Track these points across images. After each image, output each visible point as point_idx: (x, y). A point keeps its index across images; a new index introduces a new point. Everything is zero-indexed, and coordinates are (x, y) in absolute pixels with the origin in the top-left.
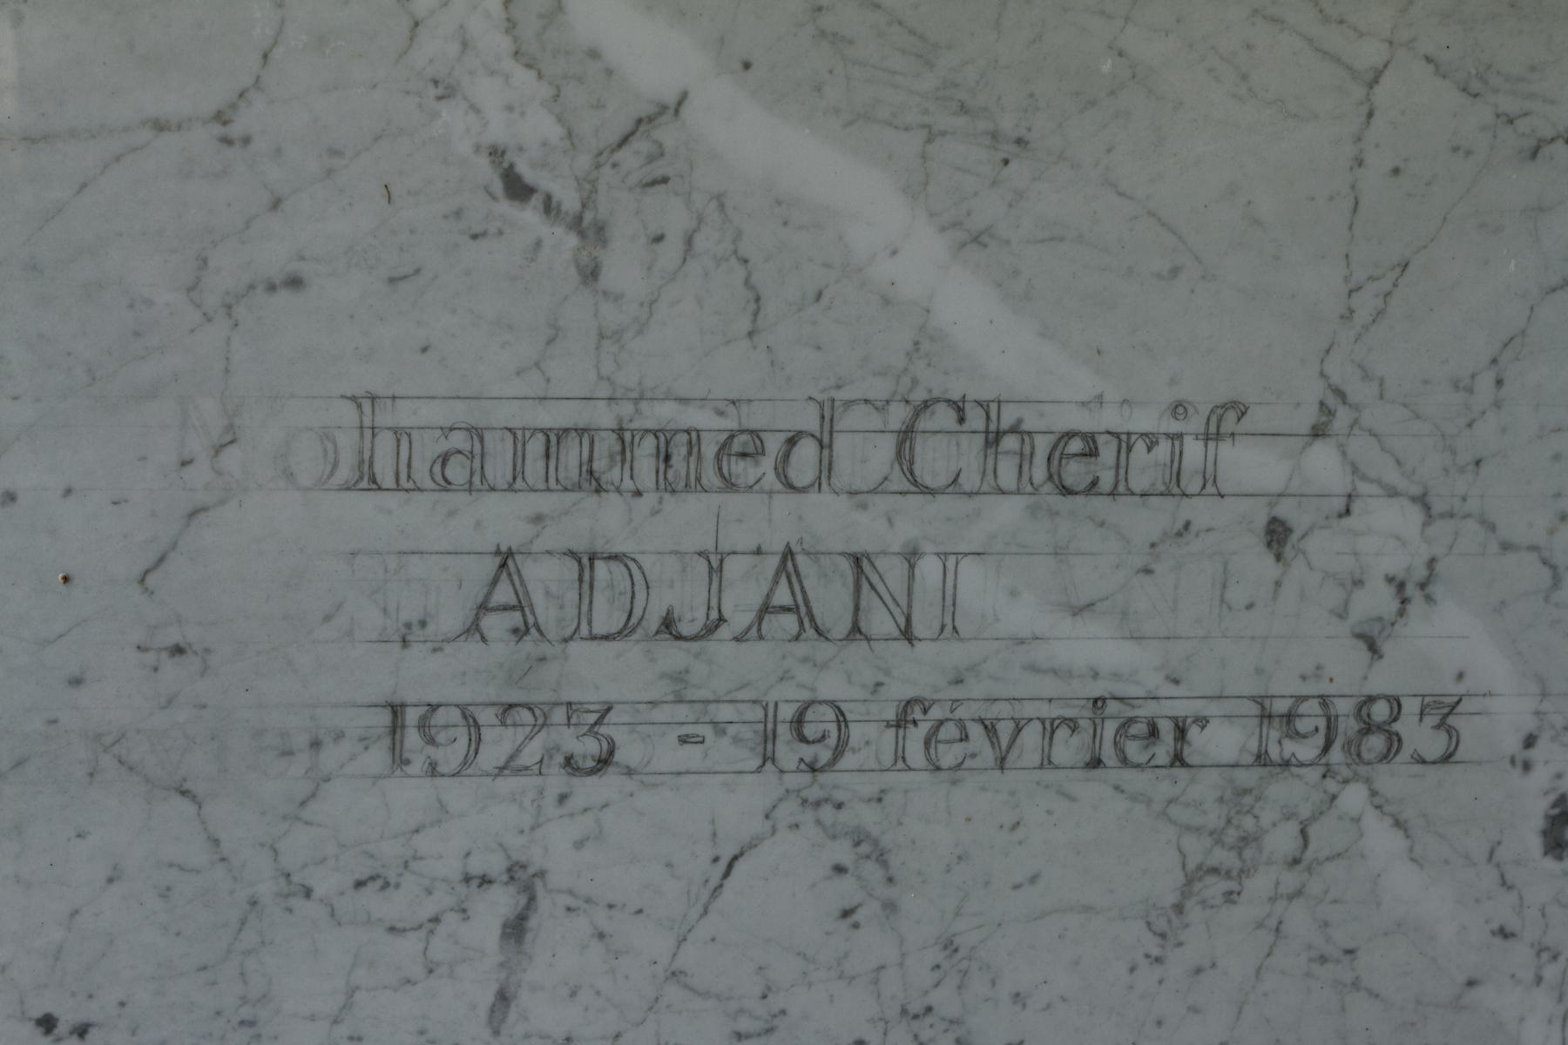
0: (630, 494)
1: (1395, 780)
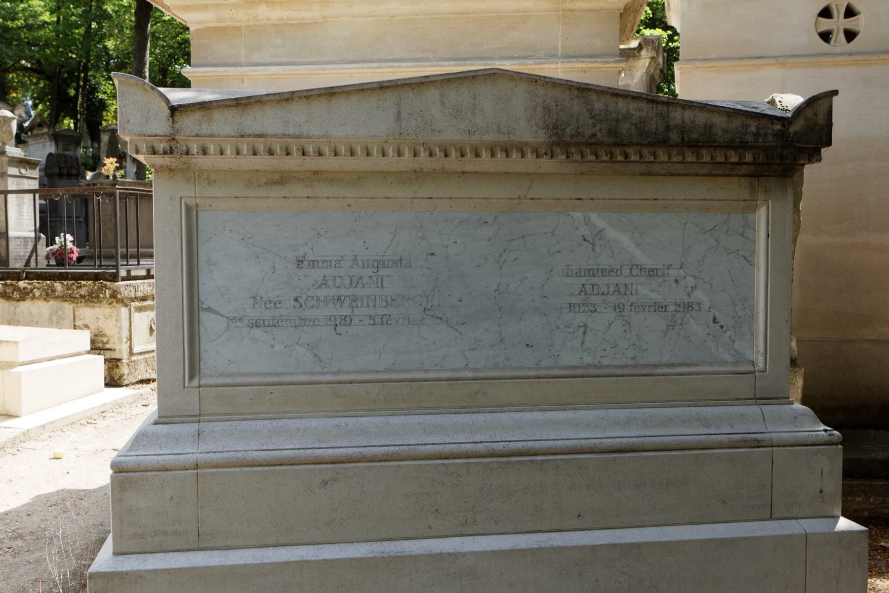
1: (693, 313)
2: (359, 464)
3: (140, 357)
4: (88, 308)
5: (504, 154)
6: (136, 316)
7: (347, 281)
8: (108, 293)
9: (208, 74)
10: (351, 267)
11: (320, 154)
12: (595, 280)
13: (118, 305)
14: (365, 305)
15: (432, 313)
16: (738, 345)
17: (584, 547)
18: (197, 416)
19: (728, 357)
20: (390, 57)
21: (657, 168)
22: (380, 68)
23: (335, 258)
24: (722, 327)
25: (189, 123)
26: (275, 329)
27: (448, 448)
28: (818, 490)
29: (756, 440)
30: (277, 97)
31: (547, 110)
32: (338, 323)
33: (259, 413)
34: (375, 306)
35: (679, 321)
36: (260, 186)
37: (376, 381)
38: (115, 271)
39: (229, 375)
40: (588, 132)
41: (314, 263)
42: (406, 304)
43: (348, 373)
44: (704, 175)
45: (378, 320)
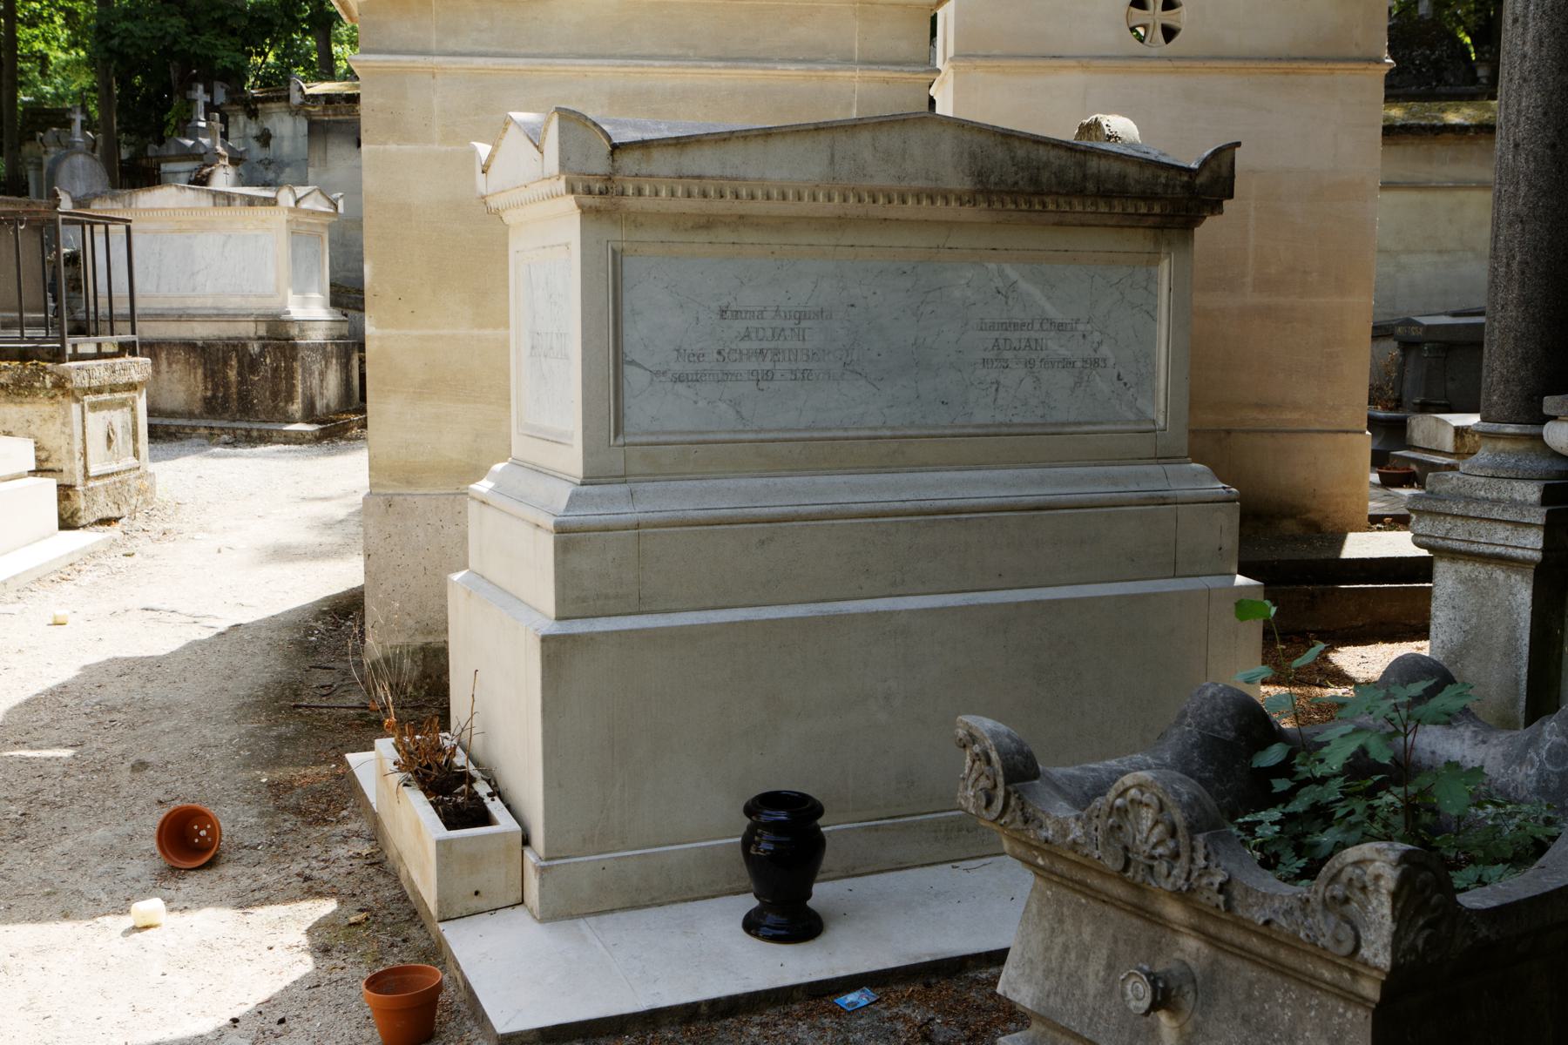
0: (208, 100)
1: (1099, 370)
2: (794, 523)
3: (98, 483)
4: (12, 405)
5: (930, 202)
6: (90, 416)
7: (769, 333)
8: (48, 381)
9: (387, 64)
10: (773, 318)
11: (753, 197)
12: (1008, 334)
13: (66, 400)
14: (787, 359)
15: (851, 368)
16: (1139, 403)
17: (1009, 604)
18: (622, 476)
19: (1131, 416)
20: (637, 52)
21: (1069, 218)
22: (626, 66)
23: (758, 309)
24: (1125, 384)
25: (628, 162)
26: (698, 384)
27: (878, 506)
28: (1217, 547)
29: (1162, 497)
30: (716, 137)
31: (973, 156)
32: (760, 377)
33: (685, 474)
34: (796, 360)
35: (1086, 378)
36: (686, 230)
37: (798, 440)
38: (58, 345)
39: (652, 433)
40: (1010, 181)
41: (737, 314)
42: (826, 358)
43: (770, 431)
44: (1112, 226)
45: (799, 375)
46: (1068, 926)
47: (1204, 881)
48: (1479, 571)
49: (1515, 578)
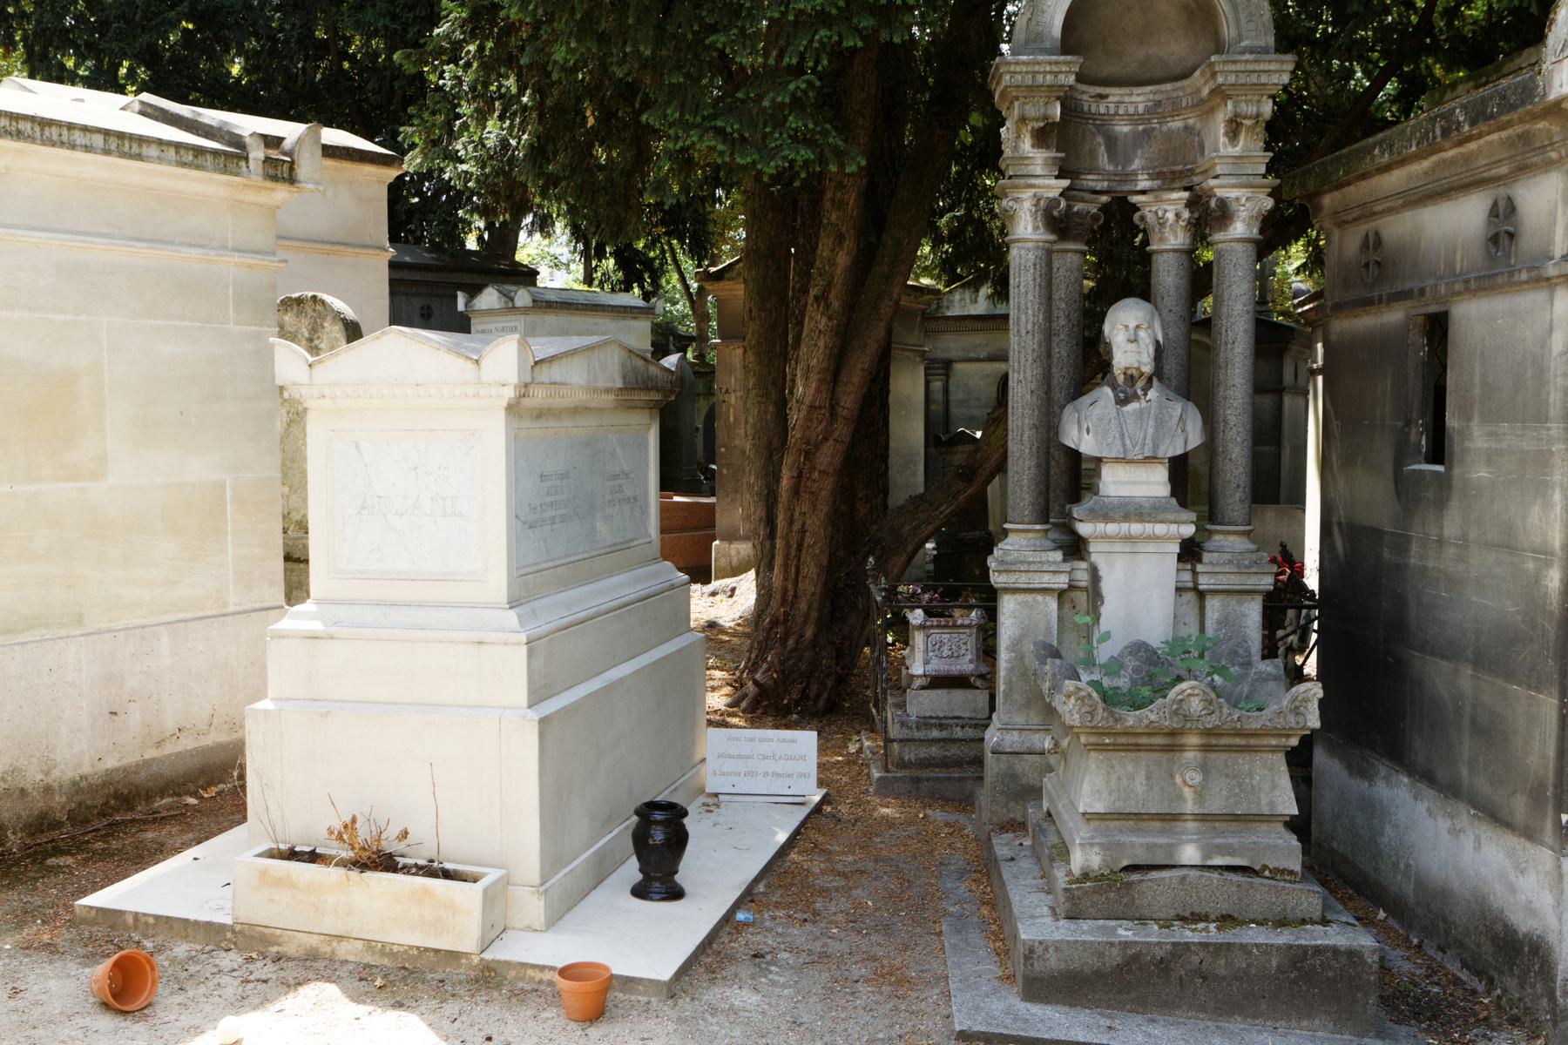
27: (624, 600)
46: (1118, 767)
47: (1229, 719)
48: (1029, 597)
49: (1048, 598)
